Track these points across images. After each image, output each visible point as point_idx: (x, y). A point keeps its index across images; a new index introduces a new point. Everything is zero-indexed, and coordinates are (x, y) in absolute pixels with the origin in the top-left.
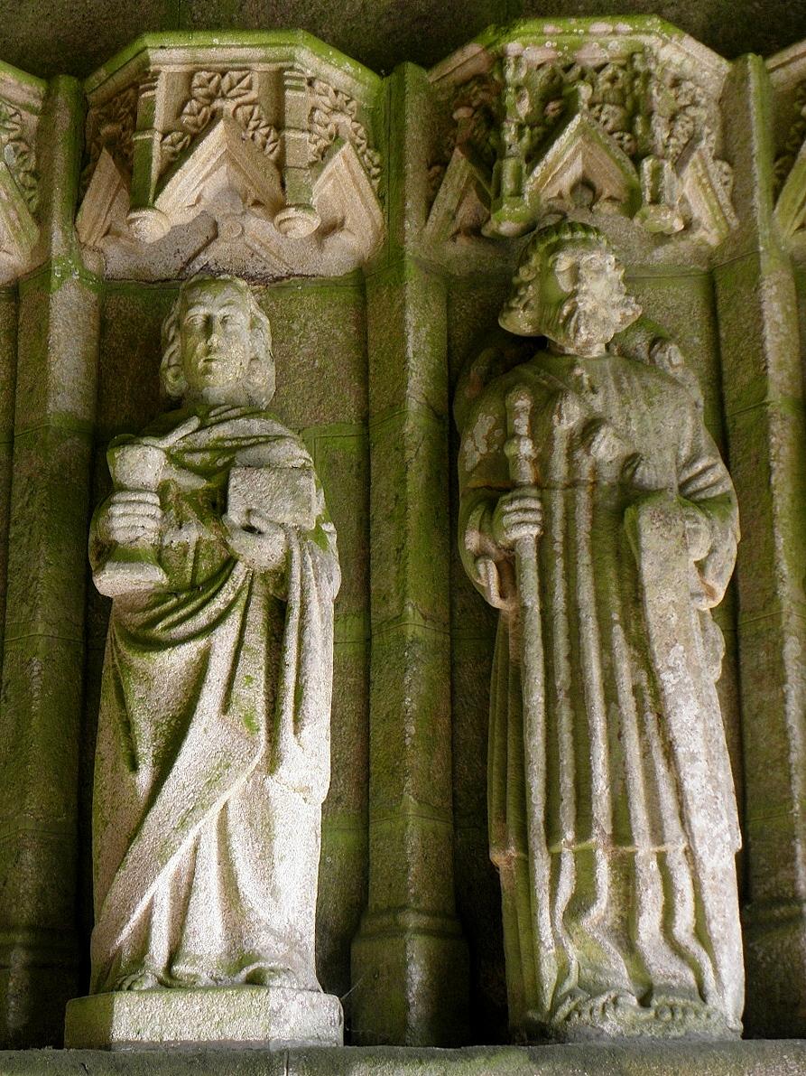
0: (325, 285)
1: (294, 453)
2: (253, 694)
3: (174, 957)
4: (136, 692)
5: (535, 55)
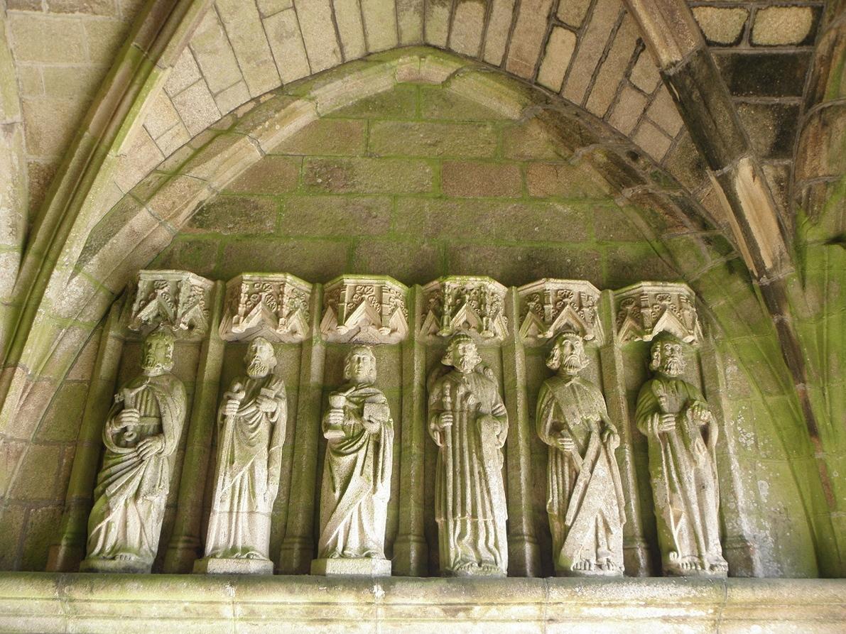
0: (391, 347)
1: (382, 398)
2: (369, 470)
3: (344, 548)
4: (335, 468)
5: (453, 285)
